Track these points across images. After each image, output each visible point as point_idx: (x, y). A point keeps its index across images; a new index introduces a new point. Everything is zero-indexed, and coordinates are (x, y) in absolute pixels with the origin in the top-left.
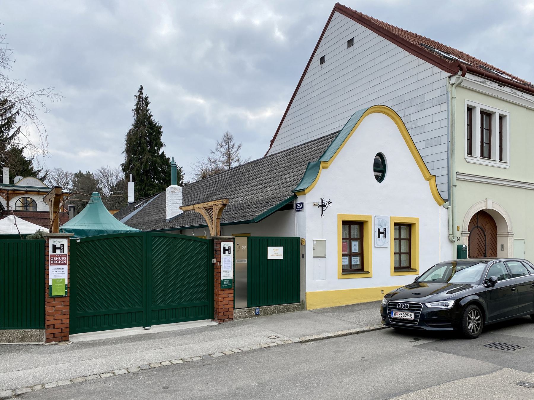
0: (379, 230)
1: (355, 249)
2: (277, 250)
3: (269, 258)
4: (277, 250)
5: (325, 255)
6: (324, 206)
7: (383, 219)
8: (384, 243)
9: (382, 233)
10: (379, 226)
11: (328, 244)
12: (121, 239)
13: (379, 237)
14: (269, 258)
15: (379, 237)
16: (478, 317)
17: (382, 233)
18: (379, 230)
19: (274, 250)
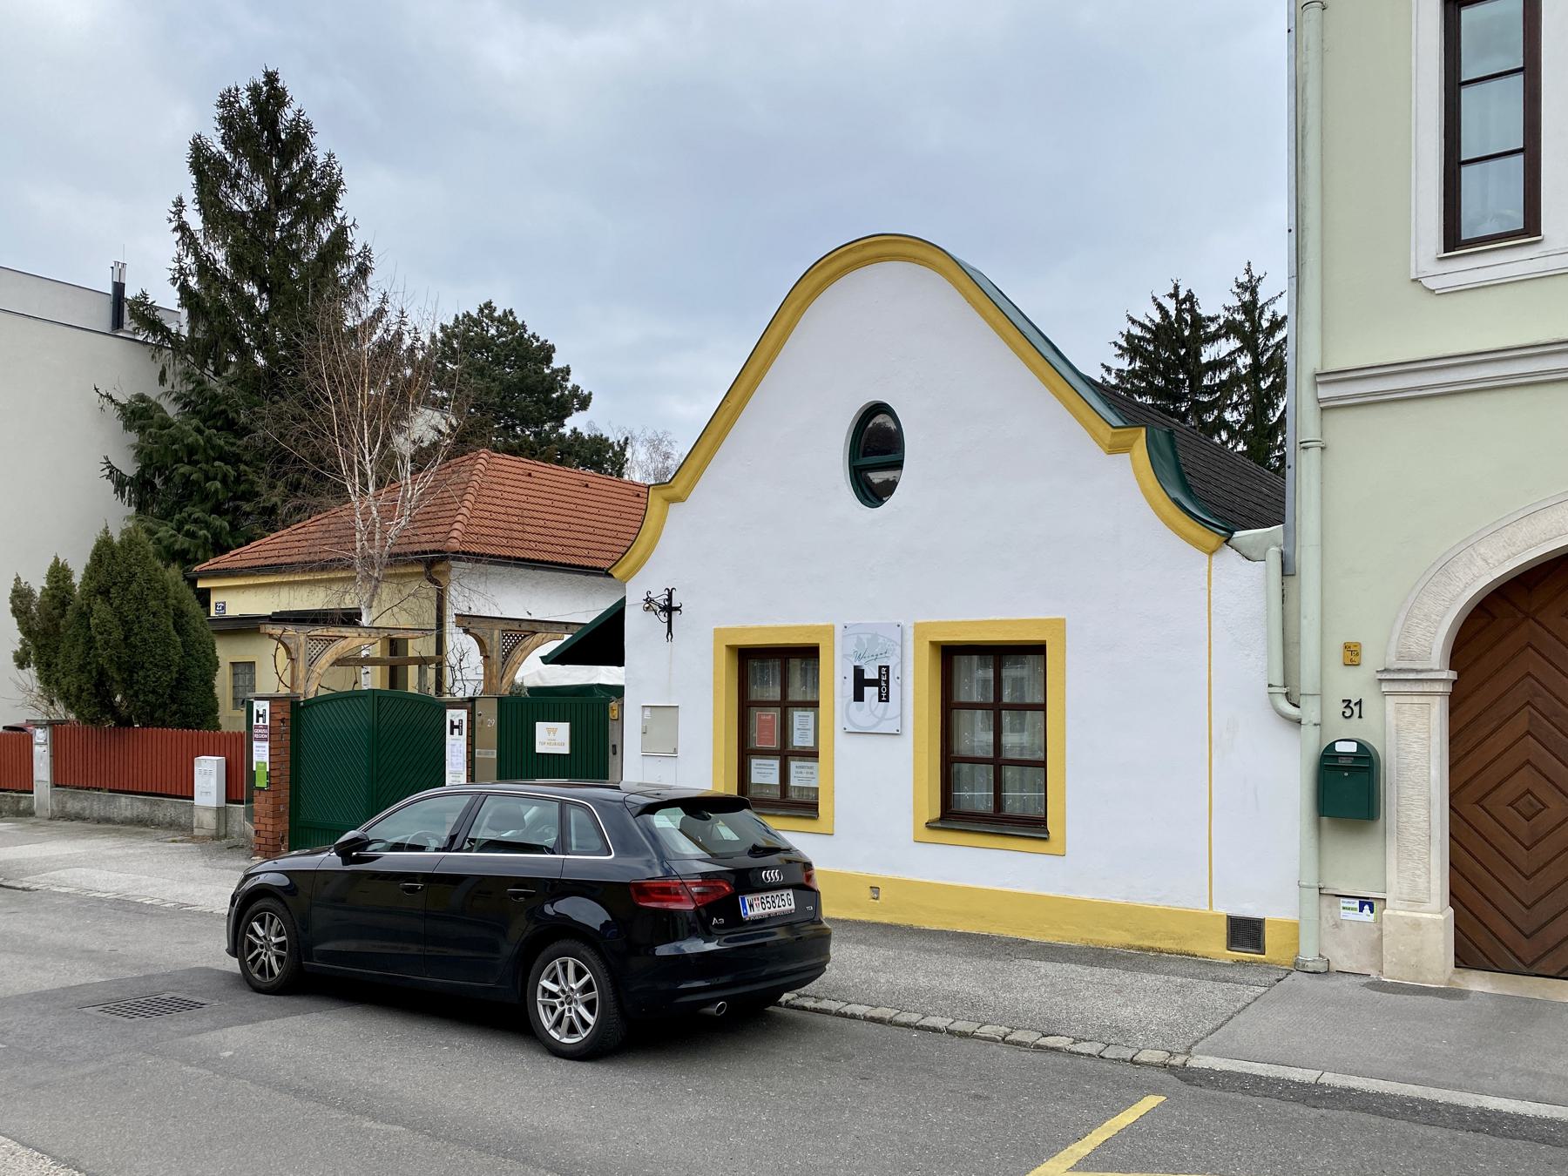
0: (859, 672)
1: (803, 736)
2: (555, 731)
3: (538, 750)
4: (555, 731)
5: (675, 751)
6: (663, 609)
7: (875, 636)
8: (881, 719)
9: (872, 683)
10: (859, 658)
11: (683, 718)
12: (617, 556)
13: (859, 697)
14: (538, 750)
15: (859, 697)
16: (283, 938)
17: (872, 683)
18: (859, 672)
19: (1476, 578)
